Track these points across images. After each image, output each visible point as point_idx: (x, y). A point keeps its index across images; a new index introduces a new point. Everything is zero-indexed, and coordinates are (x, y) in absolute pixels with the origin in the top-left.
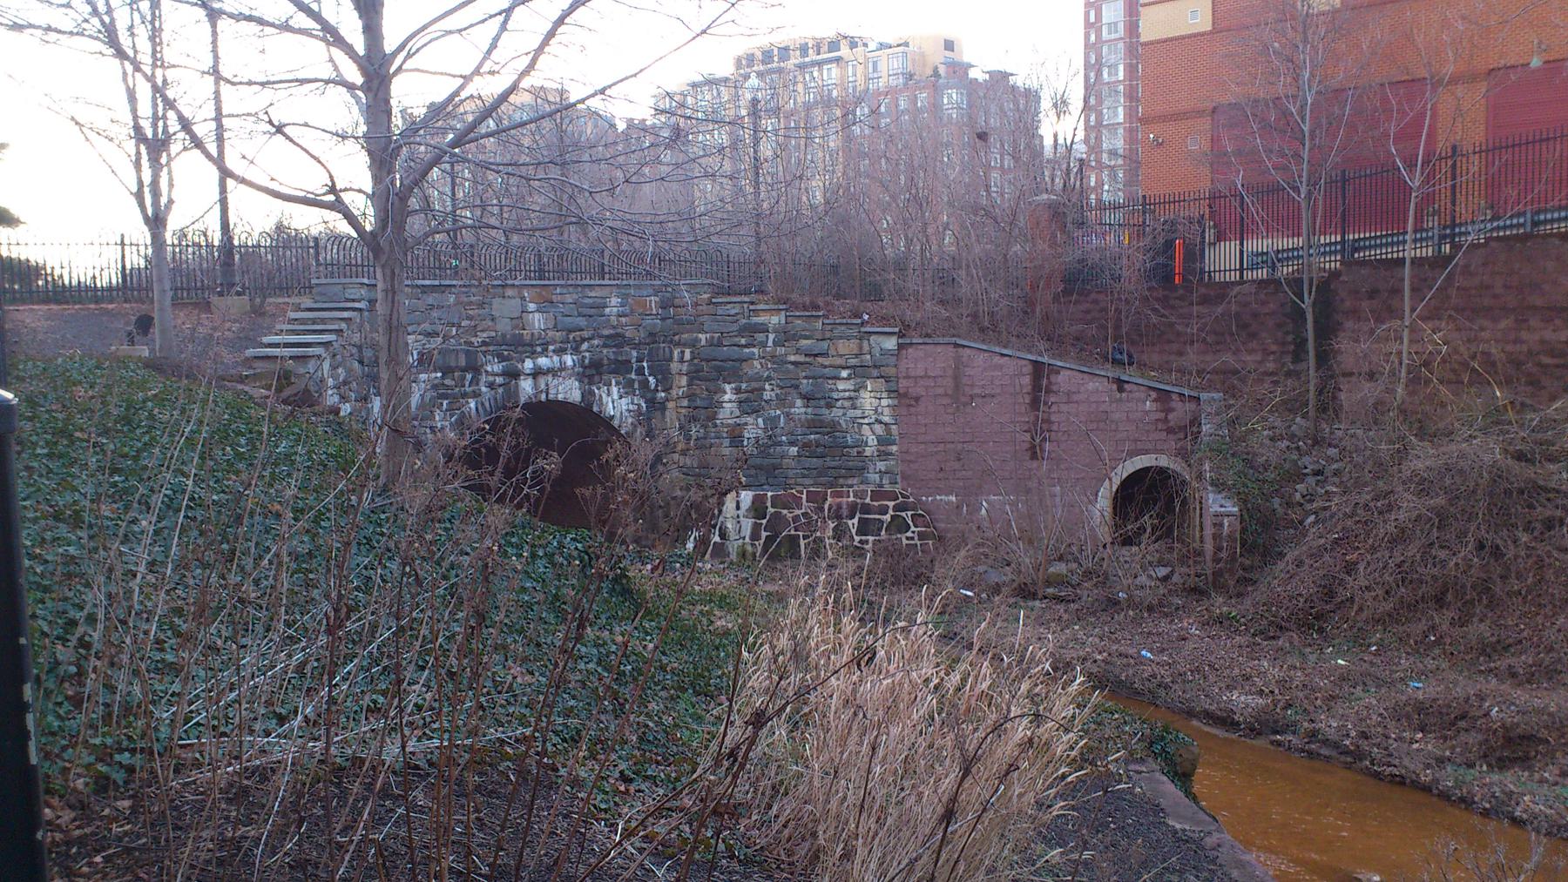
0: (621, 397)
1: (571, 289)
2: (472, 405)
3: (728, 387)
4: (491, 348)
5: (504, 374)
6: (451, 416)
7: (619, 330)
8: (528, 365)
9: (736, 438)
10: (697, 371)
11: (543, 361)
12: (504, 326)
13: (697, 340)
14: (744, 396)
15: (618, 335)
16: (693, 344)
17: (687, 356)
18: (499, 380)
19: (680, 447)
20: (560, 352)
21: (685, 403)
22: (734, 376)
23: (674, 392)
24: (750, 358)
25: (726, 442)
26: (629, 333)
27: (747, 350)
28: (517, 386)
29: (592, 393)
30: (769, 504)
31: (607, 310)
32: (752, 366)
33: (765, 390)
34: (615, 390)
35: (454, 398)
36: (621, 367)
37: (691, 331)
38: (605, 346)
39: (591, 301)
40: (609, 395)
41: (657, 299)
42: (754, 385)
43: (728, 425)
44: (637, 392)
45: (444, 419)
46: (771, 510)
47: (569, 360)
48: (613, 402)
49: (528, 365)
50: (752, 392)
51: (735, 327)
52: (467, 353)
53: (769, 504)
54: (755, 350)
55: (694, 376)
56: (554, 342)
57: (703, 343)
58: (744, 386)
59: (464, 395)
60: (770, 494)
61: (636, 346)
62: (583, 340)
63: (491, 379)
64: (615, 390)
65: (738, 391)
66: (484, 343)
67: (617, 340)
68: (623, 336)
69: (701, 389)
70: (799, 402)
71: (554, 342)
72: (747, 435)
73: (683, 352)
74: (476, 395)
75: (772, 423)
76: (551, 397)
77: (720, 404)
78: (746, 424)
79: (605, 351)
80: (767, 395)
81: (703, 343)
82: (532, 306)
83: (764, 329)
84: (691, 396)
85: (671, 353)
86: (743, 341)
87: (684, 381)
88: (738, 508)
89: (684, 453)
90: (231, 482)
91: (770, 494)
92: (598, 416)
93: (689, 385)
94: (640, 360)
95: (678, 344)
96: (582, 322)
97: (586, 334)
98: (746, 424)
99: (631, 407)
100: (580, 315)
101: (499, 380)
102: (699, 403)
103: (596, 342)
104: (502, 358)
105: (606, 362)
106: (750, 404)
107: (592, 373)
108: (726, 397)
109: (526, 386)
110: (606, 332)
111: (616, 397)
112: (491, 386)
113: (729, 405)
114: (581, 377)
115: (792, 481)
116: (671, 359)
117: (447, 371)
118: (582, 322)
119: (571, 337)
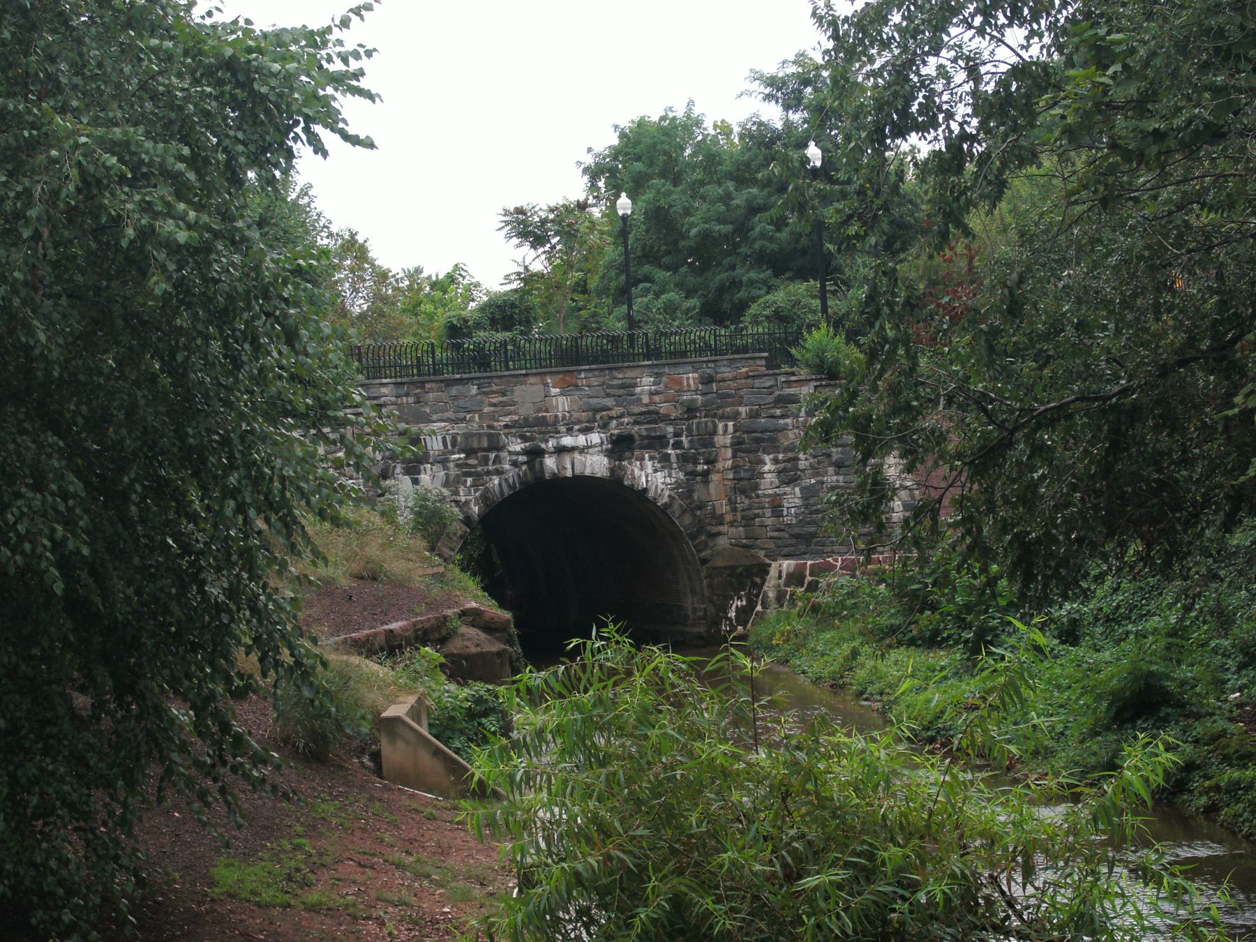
0: (656, 471)
1: (597, 373)
2: (496, 482)
3: (767, 458)
4: (513, 431)
5: (525, 452)
6: (476, 491)
7: (652, 408)
8: (551, 444)
9: (777, 509)
10: (740, 443)
11: (567, 441)
12: (526, 410)
13: (738, 414)
14: (782, 466)
15: (649, 412)
16: (735, 416)
17: (731, 429)
18: (522, 458)
19: (728, 518)
20: (586, 431)
21: (731, 476)
22: (773, 446)
23: (719, 466)
24: (784, 429)
25: (768, 513)
26: (664, 408)
27: (782, 421)
28: (542, 463)
29: (621, 468)
30: (808, 573)
31: (638, 390)
32: (787, 438)
33: (799, 459)
34: (649, 464)
35: (477, 476)
36: (655, 443)
37: (732, 404)
38: (636, 423)
39: (619, 382)
40: (642, 469)
41: (696, 375)
42: (790, 455)
43: (769, 495)
44: (675, 465)
45: (469, 494)
46: (808, 578)
47: (595, 438)
48: (647, 477)
49: (551, 444)
50: (789, 460)
51: (771, 399)
52: (490, 436)
53: (808, 573)
54: (789, 421)
55: (737, 446)
56: (579, 422)
57: (744, 415)
58: (781, 456)
59: (488, 473)
60: (809, 563)
61: (671, 422)
62: (611, 418)
63: (514, 457)
64: (649, 464)
65: (776, 461)
66: (506, 426)
67: (652, 416)
68: (657, 413)
69: (744, 460)
70: (831, 470)
71: (579, 422)
72: (786, 505)
73: (726, 426)
74: (499, 472)
75: (808, 493)
76: (577, 471)
77: (761, 475)
78: (785, 494)
79: (636, 428)
80: (802, 464)
81: (744, 415)
82: (555, 391)
83: (794, 399)
84: (735, 468)
85: (715, 426)
86: (778, 412)
87: (729, 453)
88: (780, 577)
89: (732, 524)
90: (267, 771)
91: (809, 563)
92: (631, 489)
93: (734, 456)
94: (677, 434)
95: (722, 418)
96: (609, 402)
97: (613, 413)
98: (785, 494)
99: (668, 480)
100: (608, 395)
101: (522, 458)
102: (743, 474)
103: (626, 420)
104: (524, 438)
105: (637, 437)
106: (789, 475)
107: (620, 447)
108: (766, 468)
109: (550, 462)
110: (637, 410)
111: (650, 470)
112: (515, 464)
113: (769, 476)
114: (609, 454)
115: (829, 549)
116: (715, 432)
117: (470, 452)
118: (609, 402)
119: (598, 417)
